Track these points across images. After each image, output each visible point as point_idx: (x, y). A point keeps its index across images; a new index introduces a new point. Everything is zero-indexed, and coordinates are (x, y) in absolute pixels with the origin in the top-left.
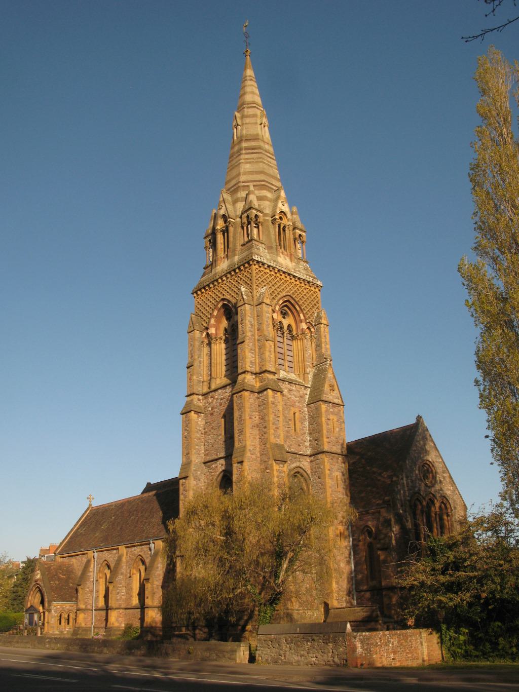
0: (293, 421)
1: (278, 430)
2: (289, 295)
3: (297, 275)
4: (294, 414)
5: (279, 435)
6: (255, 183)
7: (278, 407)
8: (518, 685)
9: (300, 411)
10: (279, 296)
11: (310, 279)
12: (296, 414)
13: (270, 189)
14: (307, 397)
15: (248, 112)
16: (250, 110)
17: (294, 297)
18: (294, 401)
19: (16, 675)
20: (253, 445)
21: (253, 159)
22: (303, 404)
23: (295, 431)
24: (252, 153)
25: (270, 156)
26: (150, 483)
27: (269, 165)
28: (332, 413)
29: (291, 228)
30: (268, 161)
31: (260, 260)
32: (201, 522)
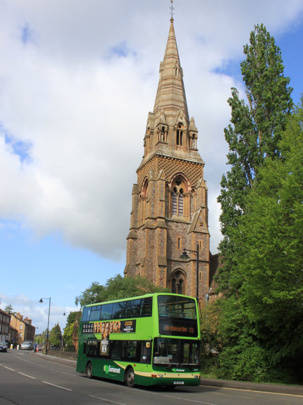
0: (178, 243)
1: (163, 249)
2: (180, 172)
3: (189, 160)
4: (179, 239)
5: (164, 252)
6: (164, 107)
7: (164, 236)
8: (302, 396)
9: (183, 237)
10: (174, 173)
11: (196, 161)
12: (180, 239)
13: (175, 109)
14: (189, 229)
15: (168, 61)
16: (169, 59)
17: (184, 173)
18: (179, 232)
19: (7, 368)
20: (150, 257)
21: (167, 91)
22: (185, 233)
23: (179, 248)
24: (167, 88)
25: (179, 87)
26: (221, 217)
27: (176, 94)
28: (200, 238)
29: (186, 132)
30: (176, 91)
31: (161, 154)
32: (280, 255)
